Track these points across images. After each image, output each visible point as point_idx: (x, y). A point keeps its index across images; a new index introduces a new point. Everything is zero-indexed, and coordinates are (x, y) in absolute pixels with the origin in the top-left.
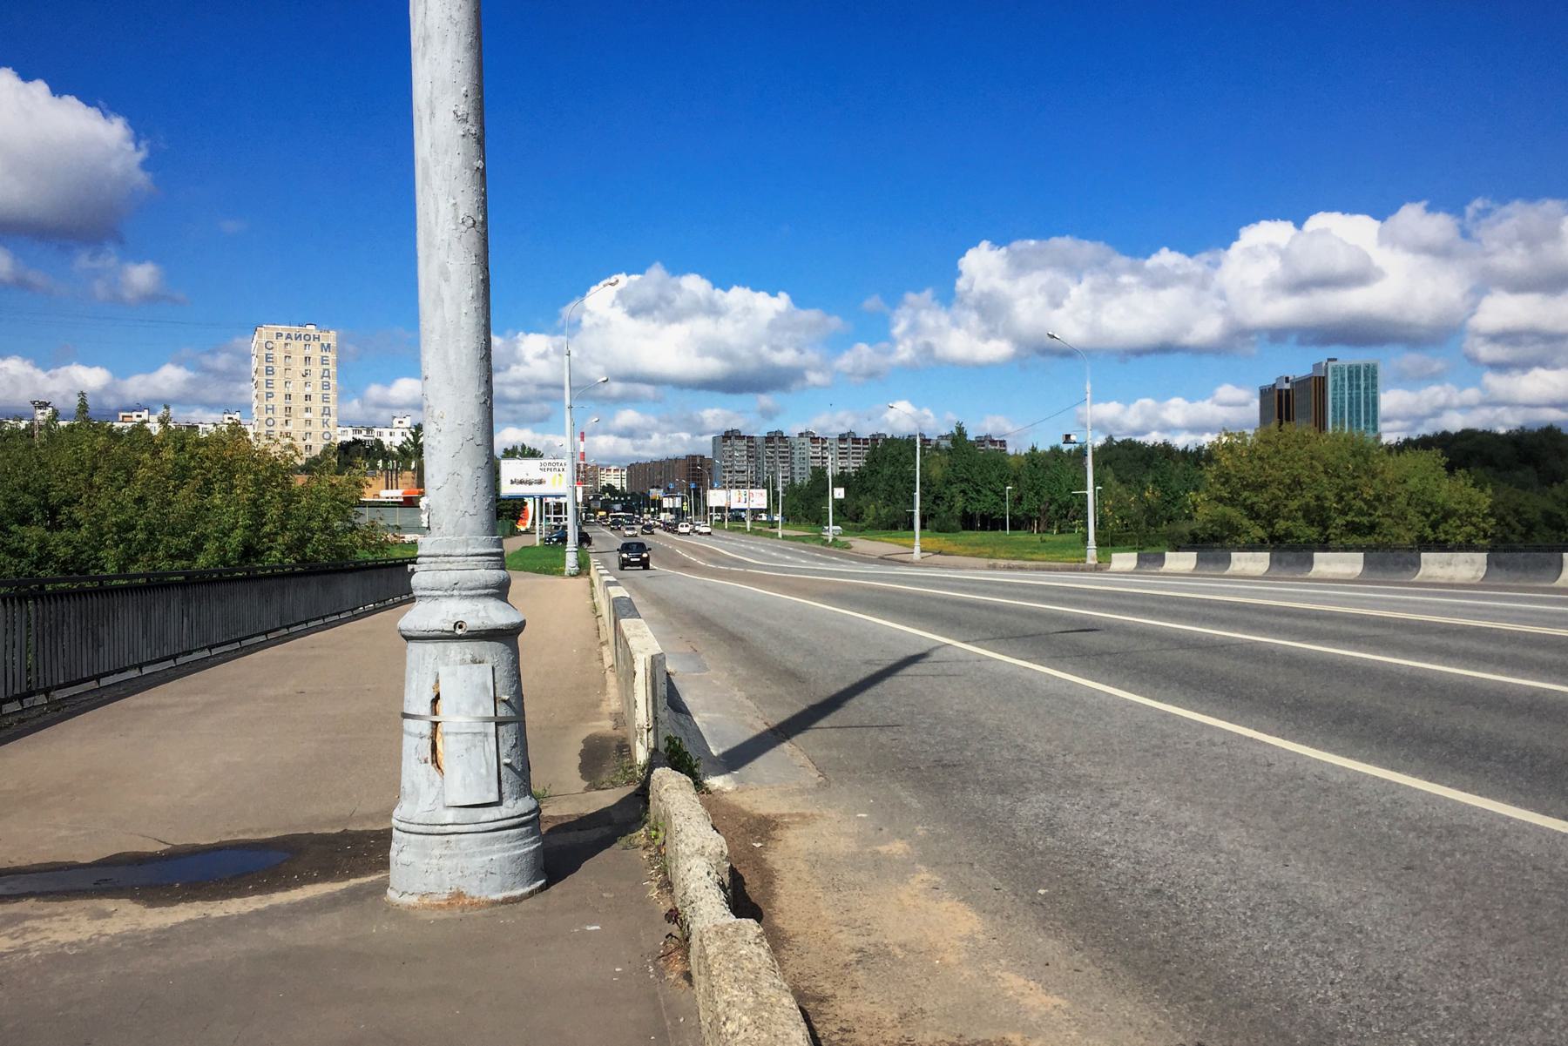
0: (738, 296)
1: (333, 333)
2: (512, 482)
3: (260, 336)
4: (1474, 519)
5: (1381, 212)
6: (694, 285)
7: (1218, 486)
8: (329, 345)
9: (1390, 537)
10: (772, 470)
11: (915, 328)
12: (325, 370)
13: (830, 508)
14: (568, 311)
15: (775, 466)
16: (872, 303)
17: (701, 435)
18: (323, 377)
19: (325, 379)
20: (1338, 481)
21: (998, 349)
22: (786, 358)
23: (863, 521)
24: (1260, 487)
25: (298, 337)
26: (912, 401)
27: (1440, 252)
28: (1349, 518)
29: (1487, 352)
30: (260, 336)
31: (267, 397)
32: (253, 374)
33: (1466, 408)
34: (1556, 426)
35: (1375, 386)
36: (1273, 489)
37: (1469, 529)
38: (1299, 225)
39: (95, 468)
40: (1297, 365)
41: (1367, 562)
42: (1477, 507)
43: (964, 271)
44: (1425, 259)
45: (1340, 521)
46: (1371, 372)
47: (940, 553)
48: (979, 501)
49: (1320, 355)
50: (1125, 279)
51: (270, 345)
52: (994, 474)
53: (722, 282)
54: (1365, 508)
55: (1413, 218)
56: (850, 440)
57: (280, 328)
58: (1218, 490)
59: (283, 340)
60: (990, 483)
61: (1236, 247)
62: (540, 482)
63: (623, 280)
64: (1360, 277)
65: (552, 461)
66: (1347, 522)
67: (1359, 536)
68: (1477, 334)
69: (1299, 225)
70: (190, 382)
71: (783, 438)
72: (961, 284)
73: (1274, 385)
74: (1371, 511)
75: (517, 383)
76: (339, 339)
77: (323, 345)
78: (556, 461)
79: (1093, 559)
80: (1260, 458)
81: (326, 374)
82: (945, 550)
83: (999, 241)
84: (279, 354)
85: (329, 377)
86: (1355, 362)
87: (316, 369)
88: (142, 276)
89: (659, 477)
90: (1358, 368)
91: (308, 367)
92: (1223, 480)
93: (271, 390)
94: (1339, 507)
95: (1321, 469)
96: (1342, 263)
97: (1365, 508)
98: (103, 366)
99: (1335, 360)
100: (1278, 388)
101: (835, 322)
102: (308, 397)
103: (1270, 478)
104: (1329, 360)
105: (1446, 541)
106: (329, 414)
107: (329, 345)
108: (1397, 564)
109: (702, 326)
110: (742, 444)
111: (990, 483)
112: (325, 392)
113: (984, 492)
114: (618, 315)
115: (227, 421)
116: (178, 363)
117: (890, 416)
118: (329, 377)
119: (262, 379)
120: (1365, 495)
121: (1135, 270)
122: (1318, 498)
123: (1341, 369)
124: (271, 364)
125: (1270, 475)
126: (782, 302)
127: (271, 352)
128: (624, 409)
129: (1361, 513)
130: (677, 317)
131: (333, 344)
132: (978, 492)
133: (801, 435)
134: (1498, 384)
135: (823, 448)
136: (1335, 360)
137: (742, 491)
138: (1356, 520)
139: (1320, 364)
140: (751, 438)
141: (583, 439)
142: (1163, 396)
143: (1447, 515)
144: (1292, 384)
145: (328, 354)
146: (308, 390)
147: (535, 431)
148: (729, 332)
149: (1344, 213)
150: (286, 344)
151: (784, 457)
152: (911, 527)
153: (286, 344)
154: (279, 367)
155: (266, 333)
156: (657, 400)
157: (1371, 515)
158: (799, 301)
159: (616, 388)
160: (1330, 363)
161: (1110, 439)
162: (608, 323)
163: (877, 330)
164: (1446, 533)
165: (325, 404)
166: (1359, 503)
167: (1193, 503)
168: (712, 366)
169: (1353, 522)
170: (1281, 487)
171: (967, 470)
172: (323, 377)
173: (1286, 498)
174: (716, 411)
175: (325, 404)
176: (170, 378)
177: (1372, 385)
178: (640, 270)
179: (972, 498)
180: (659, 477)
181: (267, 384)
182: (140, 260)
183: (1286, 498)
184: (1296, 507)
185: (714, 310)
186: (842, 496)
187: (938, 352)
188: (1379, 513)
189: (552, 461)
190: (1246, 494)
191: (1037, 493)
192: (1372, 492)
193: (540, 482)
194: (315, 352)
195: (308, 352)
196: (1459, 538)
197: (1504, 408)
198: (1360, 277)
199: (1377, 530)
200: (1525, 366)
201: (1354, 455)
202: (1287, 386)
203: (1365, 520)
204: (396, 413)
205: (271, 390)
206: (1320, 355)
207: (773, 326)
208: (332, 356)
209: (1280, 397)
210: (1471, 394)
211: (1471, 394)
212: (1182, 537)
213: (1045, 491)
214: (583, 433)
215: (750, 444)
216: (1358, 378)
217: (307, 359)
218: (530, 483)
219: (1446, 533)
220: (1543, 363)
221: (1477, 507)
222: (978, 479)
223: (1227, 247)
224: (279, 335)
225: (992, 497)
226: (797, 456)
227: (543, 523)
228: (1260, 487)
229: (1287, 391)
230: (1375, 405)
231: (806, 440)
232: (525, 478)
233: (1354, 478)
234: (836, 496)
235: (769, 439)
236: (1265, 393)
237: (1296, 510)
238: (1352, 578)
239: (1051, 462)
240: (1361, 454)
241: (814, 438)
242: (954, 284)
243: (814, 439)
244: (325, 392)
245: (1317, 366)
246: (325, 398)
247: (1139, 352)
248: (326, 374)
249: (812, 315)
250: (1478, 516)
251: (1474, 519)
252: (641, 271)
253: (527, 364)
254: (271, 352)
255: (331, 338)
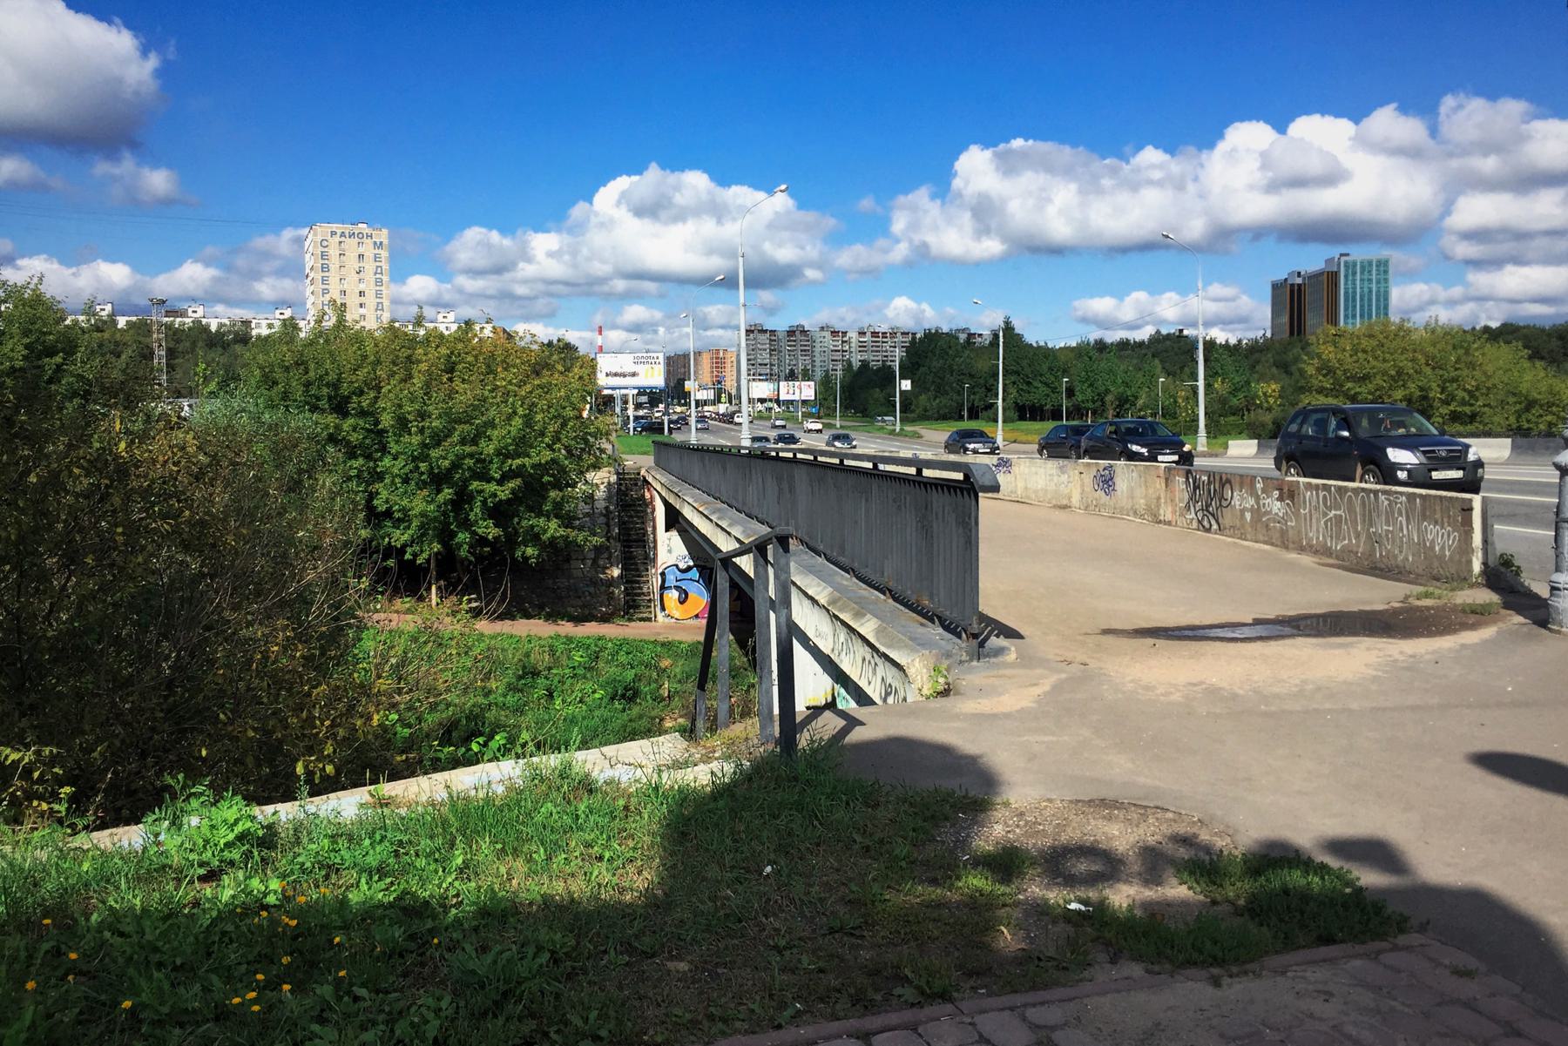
0: (741, 194)
1: (385, 232)
2: (607, 375)
3: (315, 235)
4: (1554, 409)
5: (1357, 115)
6: (696, 182)
7: (1321, 378)
8: (381, 243)
9: (1490, 426)
10: (794, 362)
11: (914, 226)
12: (377, 267)
13: (898, 399)
14: (578, 210)
15: (797, 359)
16: (867, 203)
17: (705, 330)
18: (376, 273)
19: (378, 276)
20: (1441, 372)
21: (992, 247)
22: (784, 254)
23: (913, 411)
24: (1365, 378)
25: (352, 235)
26: (911, 298)
27: (1411, 153)
28: (1452, 408)
29: (1464, 250)
30: (315, 235)
31: (323, 294)
32: (307, 271)
33: (1451, 303)
34: (1510, 321)
35: (1386, 280)
36: (1379, 381)
37: (1549, 418)
38: (1281, 128)
39: (378, 362)
40: (1311, 260)
41: (1514, 447)
42: (1557, 397)
43: (959, 173)
44: (1400, 162)
45: (1445, 410)
46: (1383, 265)
47: (1015, 442)
48: (1029, 392)
49: (1334, 251)
50: (1106, 182)
51: (325, 243)
52: (1045, 367)
53: (723, 178)
54: (1467, 398)
55: (1387, 122)
56: (869, 334)
57: (334, 227)
58: (1320, 381)
59: (337, 239)
60: (1041, 375)
61: (1222, 147)
62: (634, 375)
63: (622, 183)
64: (1331, 178)
65: (645, 355)
66: (1451, 411)
67: (1461, 424)
68: (1452, 232)
69: (1281, 128)
70: (215, 280)
71: (804, 332)
72: (957, 183)
73: (1286, 279)
74: (1472, 402)
75: (525, 281)
76: (390, 237)
77: (375, 243)
78: (649, 355)
79: (1203, 446)
80: (1364, 351)
81: (379, 271)
82: (1019, 439)
83: (987, 143)
84: (333, 252)
85: (382, 273)
86: (1367, 257)
87: (370, 266)
88: (158, 181)
89: (683, 370)
90: (1370, 263)
91: (361, 265)
92: (1324, 372)
93: (326, 287)
94: (1443, 397)
95: (1423, 361)
96: (1314, 166)
97: (1467, 398)
98: (125, 263)
99: (1348, 255)
100: (1290, 282)
101: (831, 222)
102: (361, 294)
103: (1375, 371)
104: (1342, 255)
105: (1529, 429)
106: (382, 310)
107: (381, 243)
108: (1547, 448)
109: (708, 227)
110: (764, 338)
111: (1041, 375)
112: (378, 288)
113: (1036, 384)
114: (623, 215)
115: (278, 316)
116: (207, 263)
117: (890, 313)
118: (382, 273)
119: (318, 276)
120: (1467, 386)
121: (1114, 172)
122: (1421, 389)
123: (1355, 264)
124: (326, 262)
125: (1373, 368)
126: (780, 202)
127: (326, 250)
128: (630, 305)
129: (1463, 403)
130: (681, 216)
131: (386, 242)
132: (1029, 383)
133: (822, 329)
134: (1482, 280)
135: (843, 342)
136: (1348, 255)
137: (791, 383)
138: (1459, 409)
139: (1333, 258)
140: (773, 332)
141: (600, 333)
142: (1155, 290)
143: (1530, 404)
144: (1304, 279)
145: (380, 251)
146: (362, 287)
147: (546, 326)
148: (731, 231)
149: (1323, 115)
150: (340, 242)
151: (805, 351)
152: (996, 421)
153: (340, 242)
154: (334, 263)
155: (322, 230)
156: (662, 296)
157: (1472, 405)
158: (802, 204)
159: (620, 285)
160: (1343, 259)
161: (1158, 332)
162: (612, 221)
163: (877, 227)
164: (1528, 421)
165: (379, 300)
166: (1461, 394)
167: (1265, 394)
168: (714, 264)
169: (1455, 411)
170: (1385, 378)
171: (1018, 364)
172: (376, 273)
173: (1390, 389)
174: (720, 306)
175: (379, 300)
176: (191, 276)
177: (1384, 280)
178: (639, 171)
179: (1022, 390)
180: (683, 370)
181: (323, 280)
182: (156, 164)
183: (1390, 389)
184: (1400, 397)
185: (718, 212)
186: (909, 388)
187: (934, 250)
188: (1480, 403)
189: (645, 355)
190: (1349, 385)
191: (1091, 385)
192: (1473, 383)
193: (634, 375)
194: (368, 249)
195: (361, 250)
196: (1542, 427)
197: (1492, 303)
198: (1331, 178)
199: (1478, 419)
200: (1496, 263)
201: (1454, 348)
202: (1299, 281)
203: (1467, 409)
204: (442, 310)
205: (326, 287)
206: (1334, 251)
207: (772, 226)
208: (384, 254)
209: (1292, 292)
210: (1457, 291)
211: (1457, 291)
212: (1263, 425)
213: (1100, 382)
214: (601, 327)
215: (773, 338)
216: (1354, 274)
217: (361, 256)
218: (625, 376)
219: (1528, 421)
220: (1519, 261)
221: (1557, 397)
222: (1028, 370)
223: (1211, 145)
224: (333, 233)
225: (1043, 389)
226: (817, 349)
227: (631, 412)
228: (1365, 378)
229: (1299, 285)
230: (1386, 299)
231: (827, 334)
232: (619, 371)
233: (1456, 369)
234: (903, 388)
235: (791, 333)
236: (1276, 287)
237: (1401, 401)
238: (1502, 461)
239: (1095, 354)
240: (1462, 347)
241: (835, 332)
242: (949, 184)
243: (835, 333)
244: (378, 288)
245: (1329, 261)
246: (378, 295)
247: (1146, 247)
248: (379, 271)
249: (810, 216)
250: (1558, 406)
251: (1554, 409)
252: (640, 173)
253: (539, 263)
254: (326, 250)
255: (383, 235)
